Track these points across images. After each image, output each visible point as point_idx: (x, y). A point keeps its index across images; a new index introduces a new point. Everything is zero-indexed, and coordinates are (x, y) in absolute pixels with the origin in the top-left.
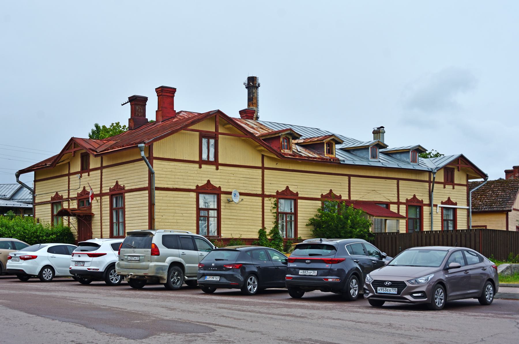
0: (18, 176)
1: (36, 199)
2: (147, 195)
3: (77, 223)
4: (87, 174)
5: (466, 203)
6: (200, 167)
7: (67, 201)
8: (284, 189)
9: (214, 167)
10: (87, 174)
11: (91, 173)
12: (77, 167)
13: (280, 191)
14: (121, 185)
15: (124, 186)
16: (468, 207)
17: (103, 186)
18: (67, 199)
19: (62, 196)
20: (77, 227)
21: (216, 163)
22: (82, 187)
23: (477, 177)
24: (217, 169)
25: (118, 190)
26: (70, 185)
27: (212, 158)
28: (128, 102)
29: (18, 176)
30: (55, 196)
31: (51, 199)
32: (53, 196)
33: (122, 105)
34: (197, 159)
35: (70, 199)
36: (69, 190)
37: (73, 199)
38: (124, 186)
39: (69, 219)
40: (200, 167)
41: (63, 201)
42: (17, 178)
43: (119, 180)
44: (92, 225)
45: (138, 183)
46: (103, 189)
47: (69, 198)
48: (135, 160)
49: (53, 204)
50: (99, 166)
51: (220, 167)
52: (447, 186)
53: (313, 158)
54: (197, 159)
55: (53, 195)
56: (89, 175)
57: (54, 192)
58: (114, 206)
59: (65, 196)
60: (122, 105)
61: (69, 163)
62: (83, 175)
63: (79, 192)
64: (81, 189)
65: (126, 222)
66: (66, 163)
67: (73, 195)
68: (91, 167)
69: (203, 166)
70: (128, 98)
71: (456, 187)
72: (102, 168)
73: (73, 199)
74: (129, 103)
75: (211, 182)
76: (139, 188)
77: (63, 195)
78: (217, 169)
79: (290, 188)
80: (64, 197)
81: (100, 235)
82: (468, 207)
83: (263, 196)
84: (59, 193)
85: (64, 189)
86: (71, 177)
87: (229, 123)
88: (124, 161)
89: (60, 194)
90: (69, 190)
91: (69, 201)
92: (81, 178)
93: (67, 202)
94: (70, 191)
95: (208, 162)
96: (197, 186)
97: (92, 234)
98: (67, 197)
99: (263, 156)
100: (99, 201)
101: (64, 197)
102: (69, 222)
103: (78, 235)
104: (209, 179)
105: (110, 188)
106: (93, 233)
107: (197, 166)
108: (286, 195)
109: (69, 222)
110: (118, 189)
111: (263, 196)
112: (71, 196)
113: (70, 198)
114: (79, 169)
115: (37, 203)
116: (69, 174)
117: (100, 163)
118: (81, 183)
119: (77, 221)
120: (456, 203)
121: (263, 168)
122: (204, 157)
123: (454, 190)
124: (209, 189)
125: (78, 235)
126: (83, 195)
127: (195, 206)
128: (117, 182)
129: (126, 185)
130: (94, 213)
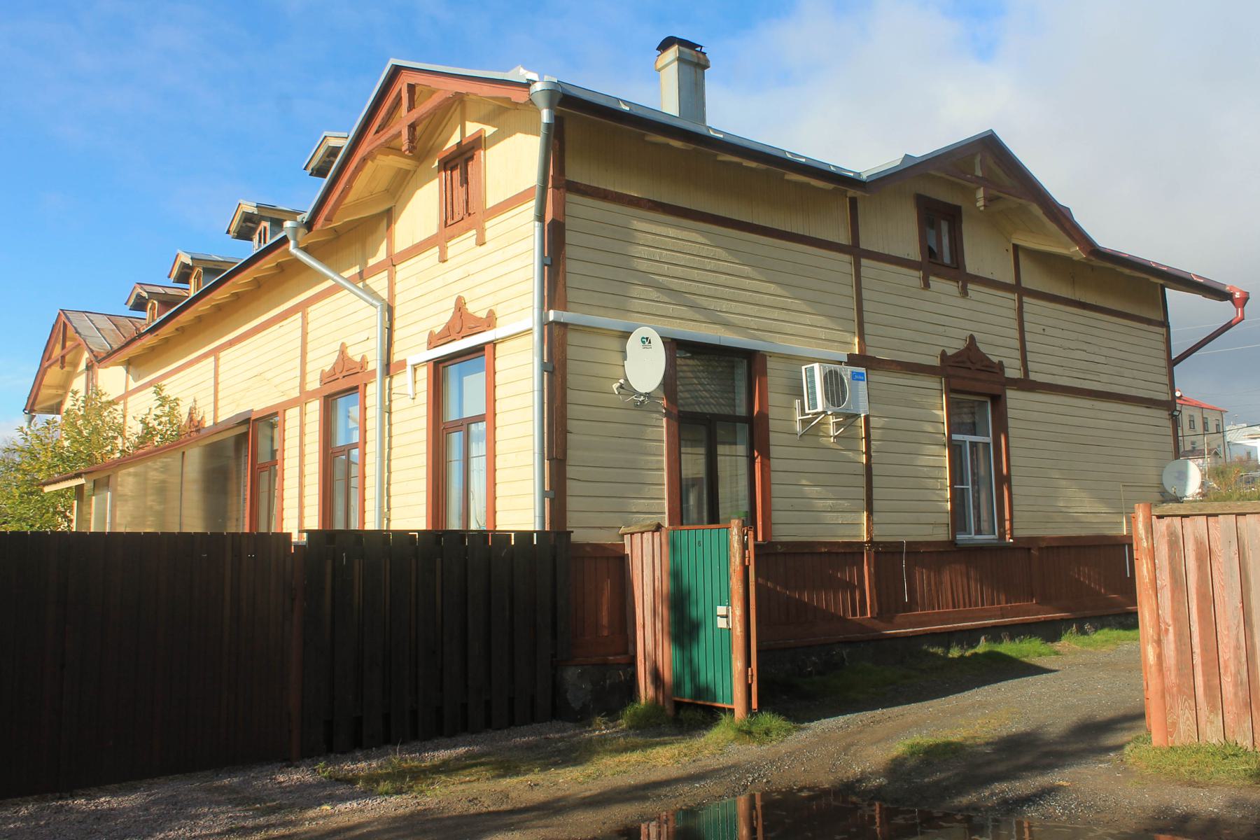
8: (961, 345)
52: (933, 281)
79: (978, 344)
107: (914, 277)
108: (970, 369)
121: (1017, 288)
123: (927, 293)
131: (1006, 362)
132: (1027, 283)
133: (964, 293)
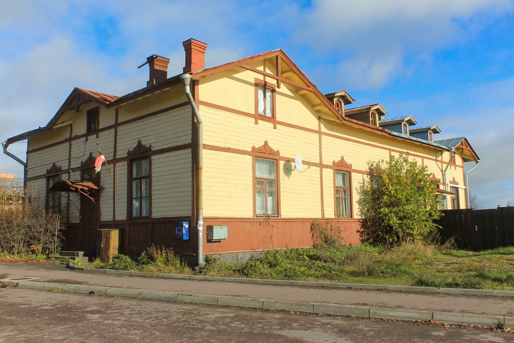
0: (6, 147)
1: (28, 173)
2: (190, 155)
3: (79, 201)
4: (95, 136)
5: (463, 184)
6: (256, 123)
7: (67, 173)
9: (271, 125)
10: (95, 136)
11: (100, 134)
12: (81, 127)
13: (336, 161)
14: (146, 146)
15: (150, 146)
16: (465, 187)
17: (118, 149)
18: (66, 170)
19: (61, 167)
20: (79, 207)
21: (273, 119)
22: (88, 153)
23: (470, 160)
24: (275, 128)
25: (140, 153)
26: (72, 153)
27: (269, 114)
28: (146, 63)
29: (6, 147)
30: (51, 168)
31: (47, 172)
32: (49, 168)
33: (139, 68)
34: (253, 112)
35: (70, 170)
36: (70, 160)
37: (74, 170)
38: (150, 146)
39: (69, 196)
40: (256, 123)
41: (62, 174)
42: (5, 149)
43: (142, 139)
44: (101, 202)
45: (174, 140)
46: (118, 153)
47: (69, 169)
48: (168, 108)
49: (48, 178)
50: (113, 123)
51: (278, 126)
54: (253, 112)
55: (49, 167)
56: (97, 137)
57: (51, 164)
58: (134, 175)
59: (65, 167)
60: (139, 68)
61: (71, 125)
62: (89, 138)
63: (84, 161)
64: (87, 157)
65: (153, 197)
66: (67, 126)
67: (76, 164)
68: (101, 127)
70: (147, 58)
72: (116, 126)
73: (74, 170)
74: (148, 64)
75: (269, 144)
76: (176, 146)
77: (63, 166)
78: (275, 128)
79: (344, 159)
80: (63, 169)
81: (113, 216)
82: (465, 187)
83: (321, 166)
84: (57, 164)
85: (63, 159)
86: (73, 142)
87: (291, 70)
88: (151, 111)
89: (58, 165)
90: (70, 160)
91: (69, 172)
92: (87, 143)
93: (67, 174)
94: (71, 160)
95: (263, 118)
97: (100, 214)
98: (67, 168)
100: (112, 170)
101: (63, 169)
102: (69, 200)
103: (80, 217)
104: (266, 139)
105: (129, 150)
106: (101, 213)
107: (253, 120)
109: (69, 200)
110: (141, 151)
111: (321, 166)
112: (72, 167)
113: (71, 169)
114: (84, 131)
115: (30, 178)
116: (70, 140)
117: (115, 119)
118: (87, 149)
119: (79, 197)
120: (458, 183)
121: (320, 133)
122: (261, 110)
124: (266, 153)
125: (80, 217)
126: (89, 164)
127: (251, 175)
128: (139, 142)
129: (153, 145)
130: (104, 187)
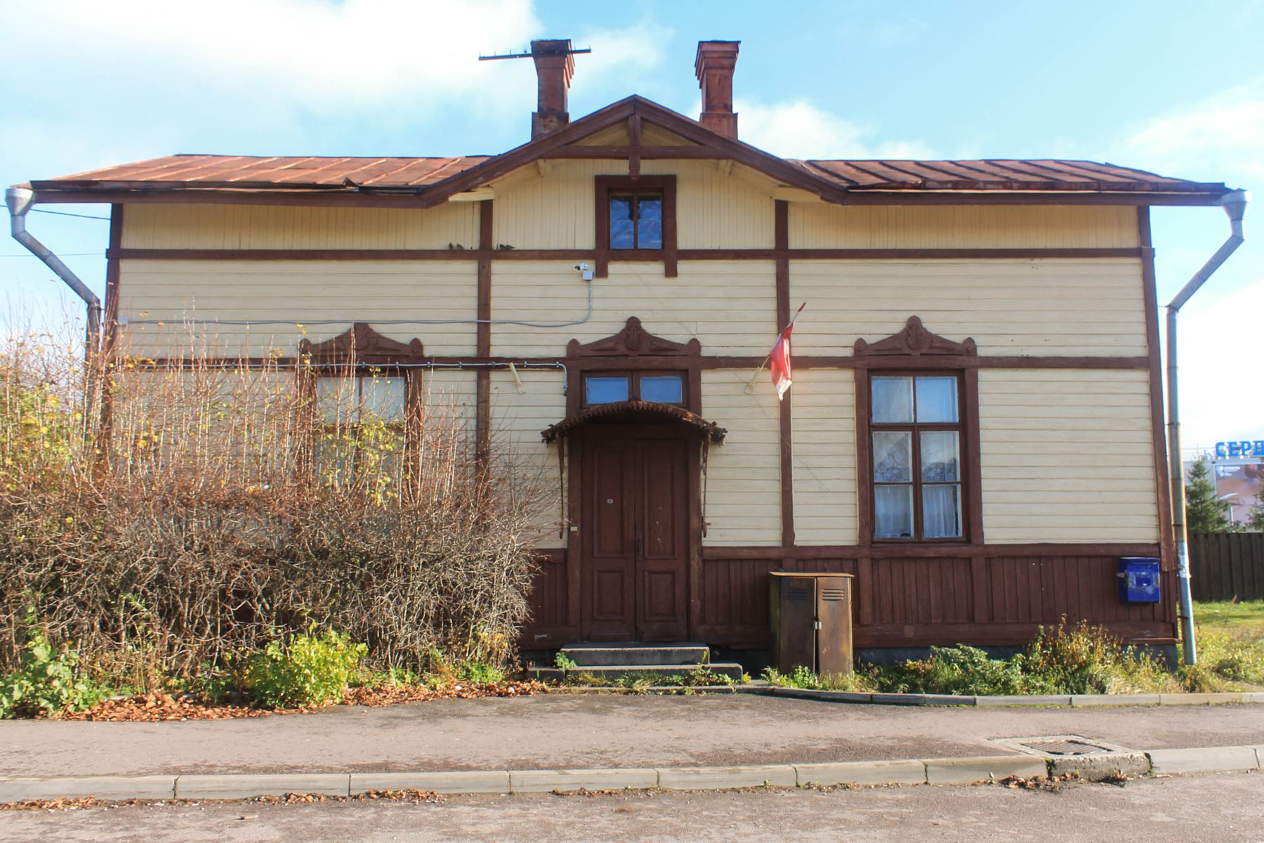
9: (658, 268)
53: (982, 185)
69: (613, 267)
71: (682, 266)
75: (644, 326)
95: (636, 254)
96: (574, 343)
99: (782, 209)
107: (588, 266)
121: (781, 254)
131: (977, 341)
132: (796, 241)
133: (671, 272)
